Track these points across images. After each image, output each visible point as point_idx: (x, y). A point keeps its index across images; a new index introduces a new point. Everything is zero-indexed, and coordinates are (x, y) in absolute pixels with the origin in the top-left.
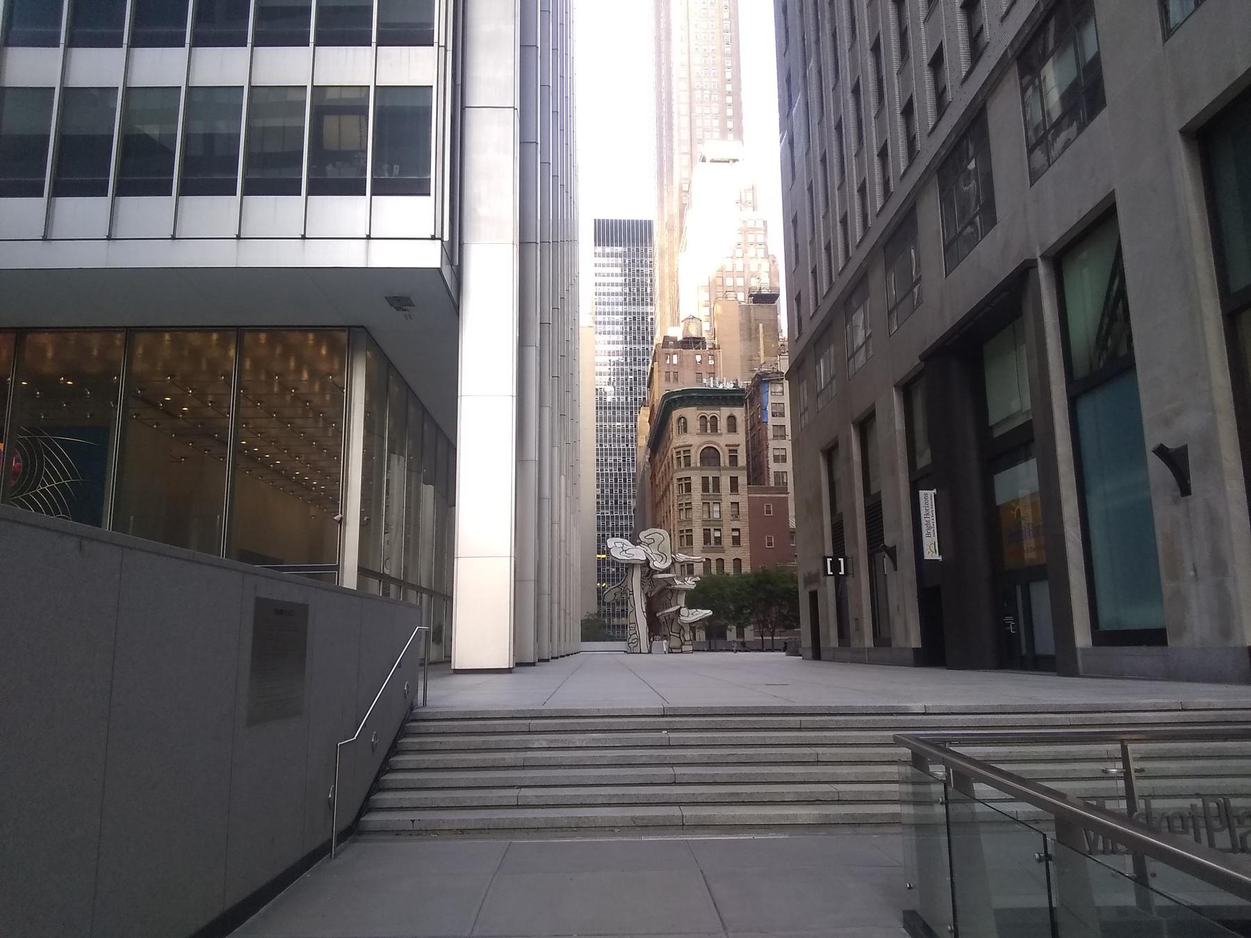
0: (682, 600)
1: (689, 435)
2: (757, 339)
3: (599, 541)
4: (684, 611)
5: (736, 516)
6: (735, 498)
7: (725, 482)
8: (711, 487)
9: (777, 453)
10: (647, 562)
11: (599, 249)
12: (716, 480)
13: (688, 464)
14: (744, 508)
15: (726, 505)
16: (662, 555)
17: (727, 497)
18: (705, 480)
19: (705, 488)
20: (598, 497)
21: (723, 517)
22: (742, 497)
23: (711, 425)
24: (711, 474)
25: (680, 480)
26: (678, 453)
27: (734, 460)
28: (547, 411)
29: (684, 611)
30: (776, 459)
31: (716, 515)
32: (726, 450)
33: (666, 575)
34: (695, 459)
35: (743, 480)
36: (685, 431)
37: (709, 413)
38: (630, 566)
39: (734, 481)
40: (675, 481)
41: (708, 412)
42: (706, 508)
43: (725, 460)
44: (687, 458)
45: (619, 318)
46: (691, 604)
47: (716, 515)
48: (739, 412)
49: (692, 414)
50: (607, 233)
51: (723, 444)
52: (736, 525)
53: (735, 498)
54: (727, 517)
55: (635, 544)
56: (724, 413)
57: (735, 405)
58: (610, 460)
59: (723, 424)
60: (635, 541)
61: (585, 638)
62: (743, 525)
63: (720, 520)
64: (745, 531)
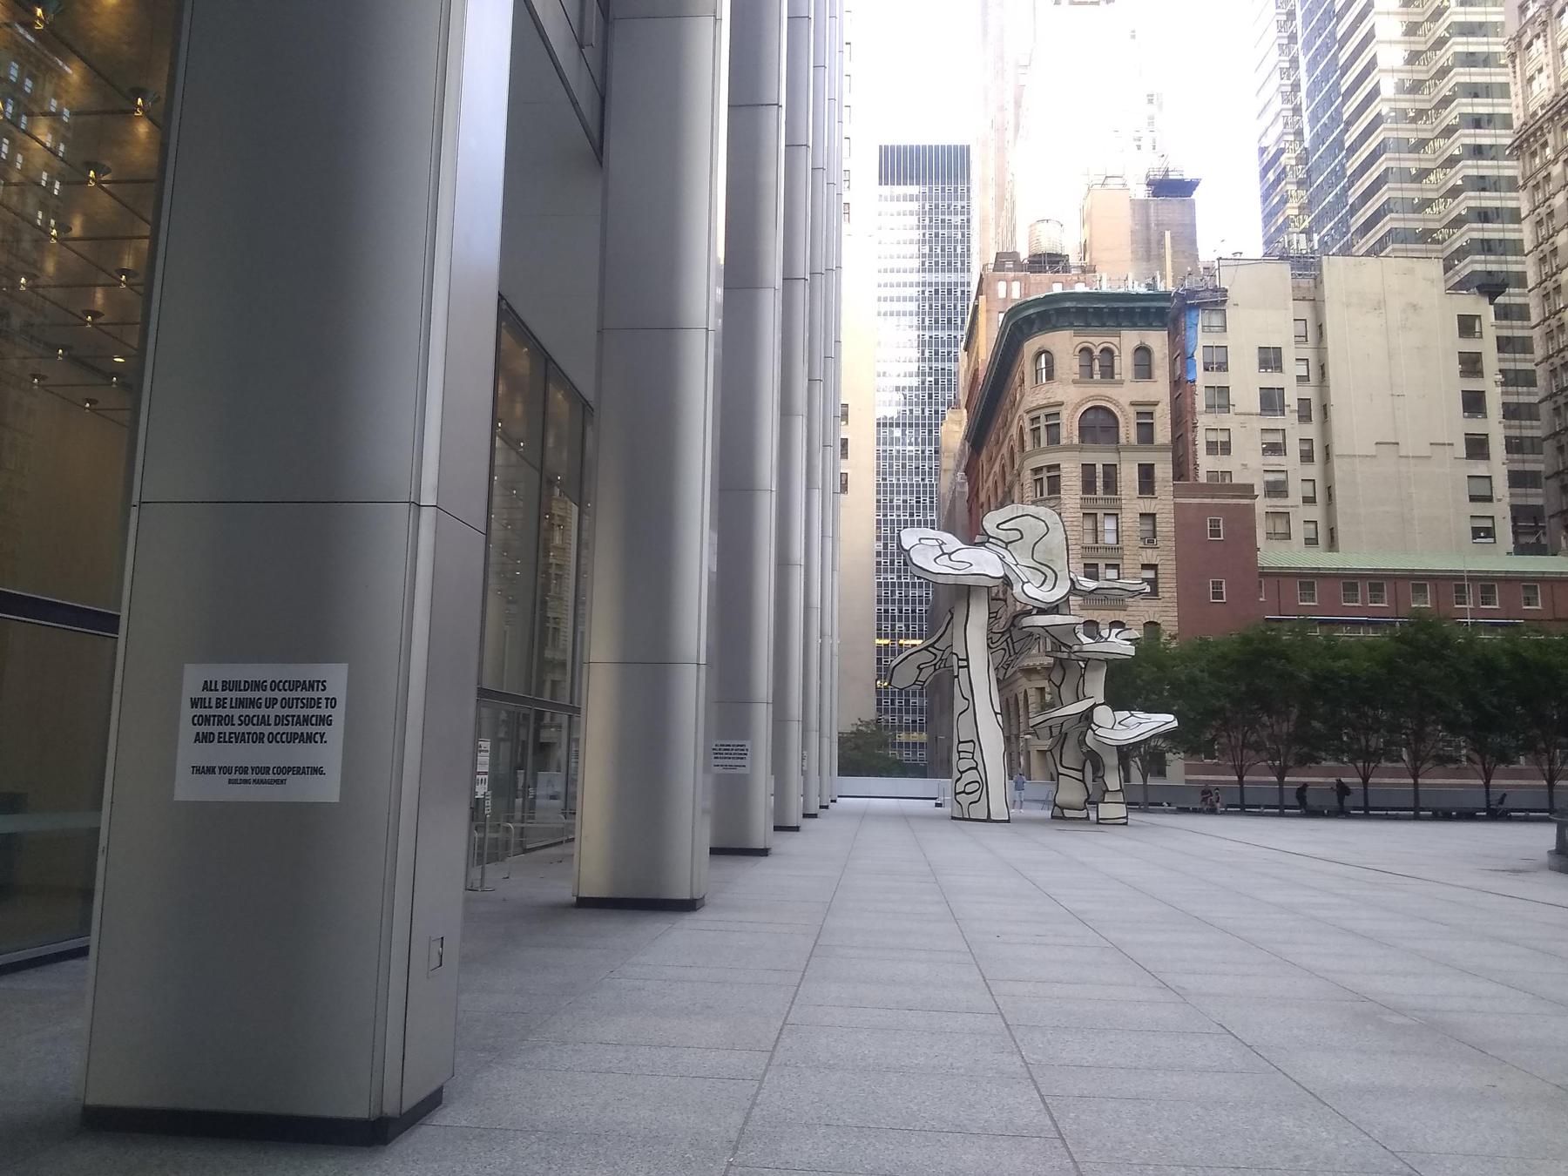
0: (1096, 686)
1: (1058, 383)
2: (1161, 258)
3: (879, 618)
4: (1103, 715)
5: (1150, 540)
6: (1147, 506)
7: (1129, 476)
8: (1099, 483)
9: (1212, 437)
10: (1006, 581)
11: (887, 190)
12: (1111, 471)
13: (1054, 439)
14: (1166, 525)
15: (1130, 518)
16: (1045, 570)
17: (1132, 503)
18: (1088, 470)
19: (1088, 485)
20: (878, 554)
21: (1125, 541)
22: (1163, 503)
23: (1100, 365)
24: (1100, 458)
25: (1037, 471)
26: (1035, 420)
27: (1146, 432)
28: (817, 494)
29: (1103, 715)
30: (1212, 447)
31: (1110, 539)
32: (1131, 412)
33: (1057, 619)
34: (1069, 429)
35: (1163, 470)
36: (1050, 376)
37: (1097, 342)
38: (962, 593)
39: (1146, 472)
40: (1027, 477)
41: (1096, 340)
42: (1089, 524)
43: (1128, 431)
44: (1053, 431)
45: (914, 292)
46: (1117, 700)
47: (1110, 539)
48: (1157, 340)
49: (1063, 343)
50: (899, 165)
51: (1124, 401)
52: (1149, 556)
53: (1147, 506)
54: (1131, 541)
55: (970, 542)
56: (1129, 339)
57: (1149, 326)
58: (898, 500)
59: (1125, 363)
60: (973, 534)
61: (849, 767)
62: (1164, 557)
63: (1117, 548)
64: (1168, 570)
